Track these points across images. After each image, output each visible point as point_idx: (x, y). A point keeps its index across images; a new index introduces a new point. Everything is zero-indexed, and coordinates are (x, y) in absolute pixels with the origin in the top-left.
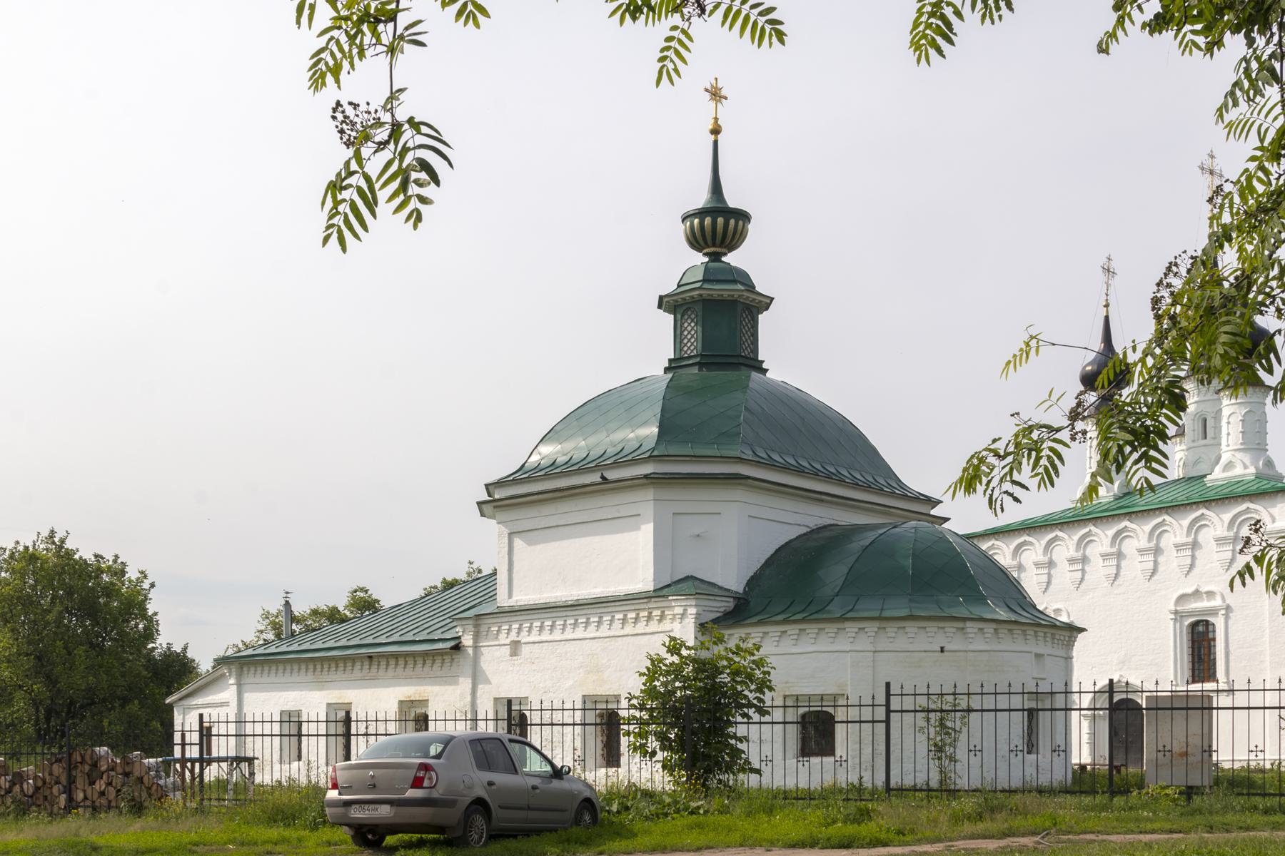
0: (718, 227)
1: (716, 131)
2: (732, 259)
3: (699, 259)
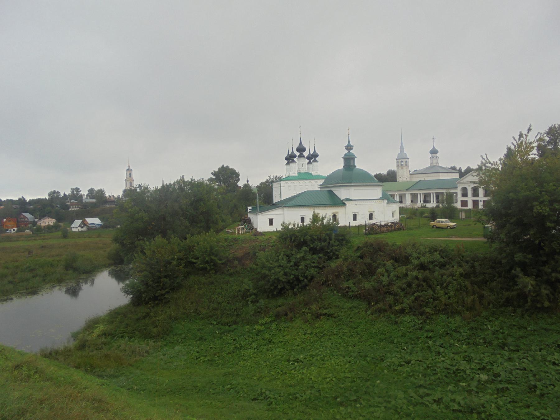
0: (349, 147)
2: (351, 151)
3: (347, 151)
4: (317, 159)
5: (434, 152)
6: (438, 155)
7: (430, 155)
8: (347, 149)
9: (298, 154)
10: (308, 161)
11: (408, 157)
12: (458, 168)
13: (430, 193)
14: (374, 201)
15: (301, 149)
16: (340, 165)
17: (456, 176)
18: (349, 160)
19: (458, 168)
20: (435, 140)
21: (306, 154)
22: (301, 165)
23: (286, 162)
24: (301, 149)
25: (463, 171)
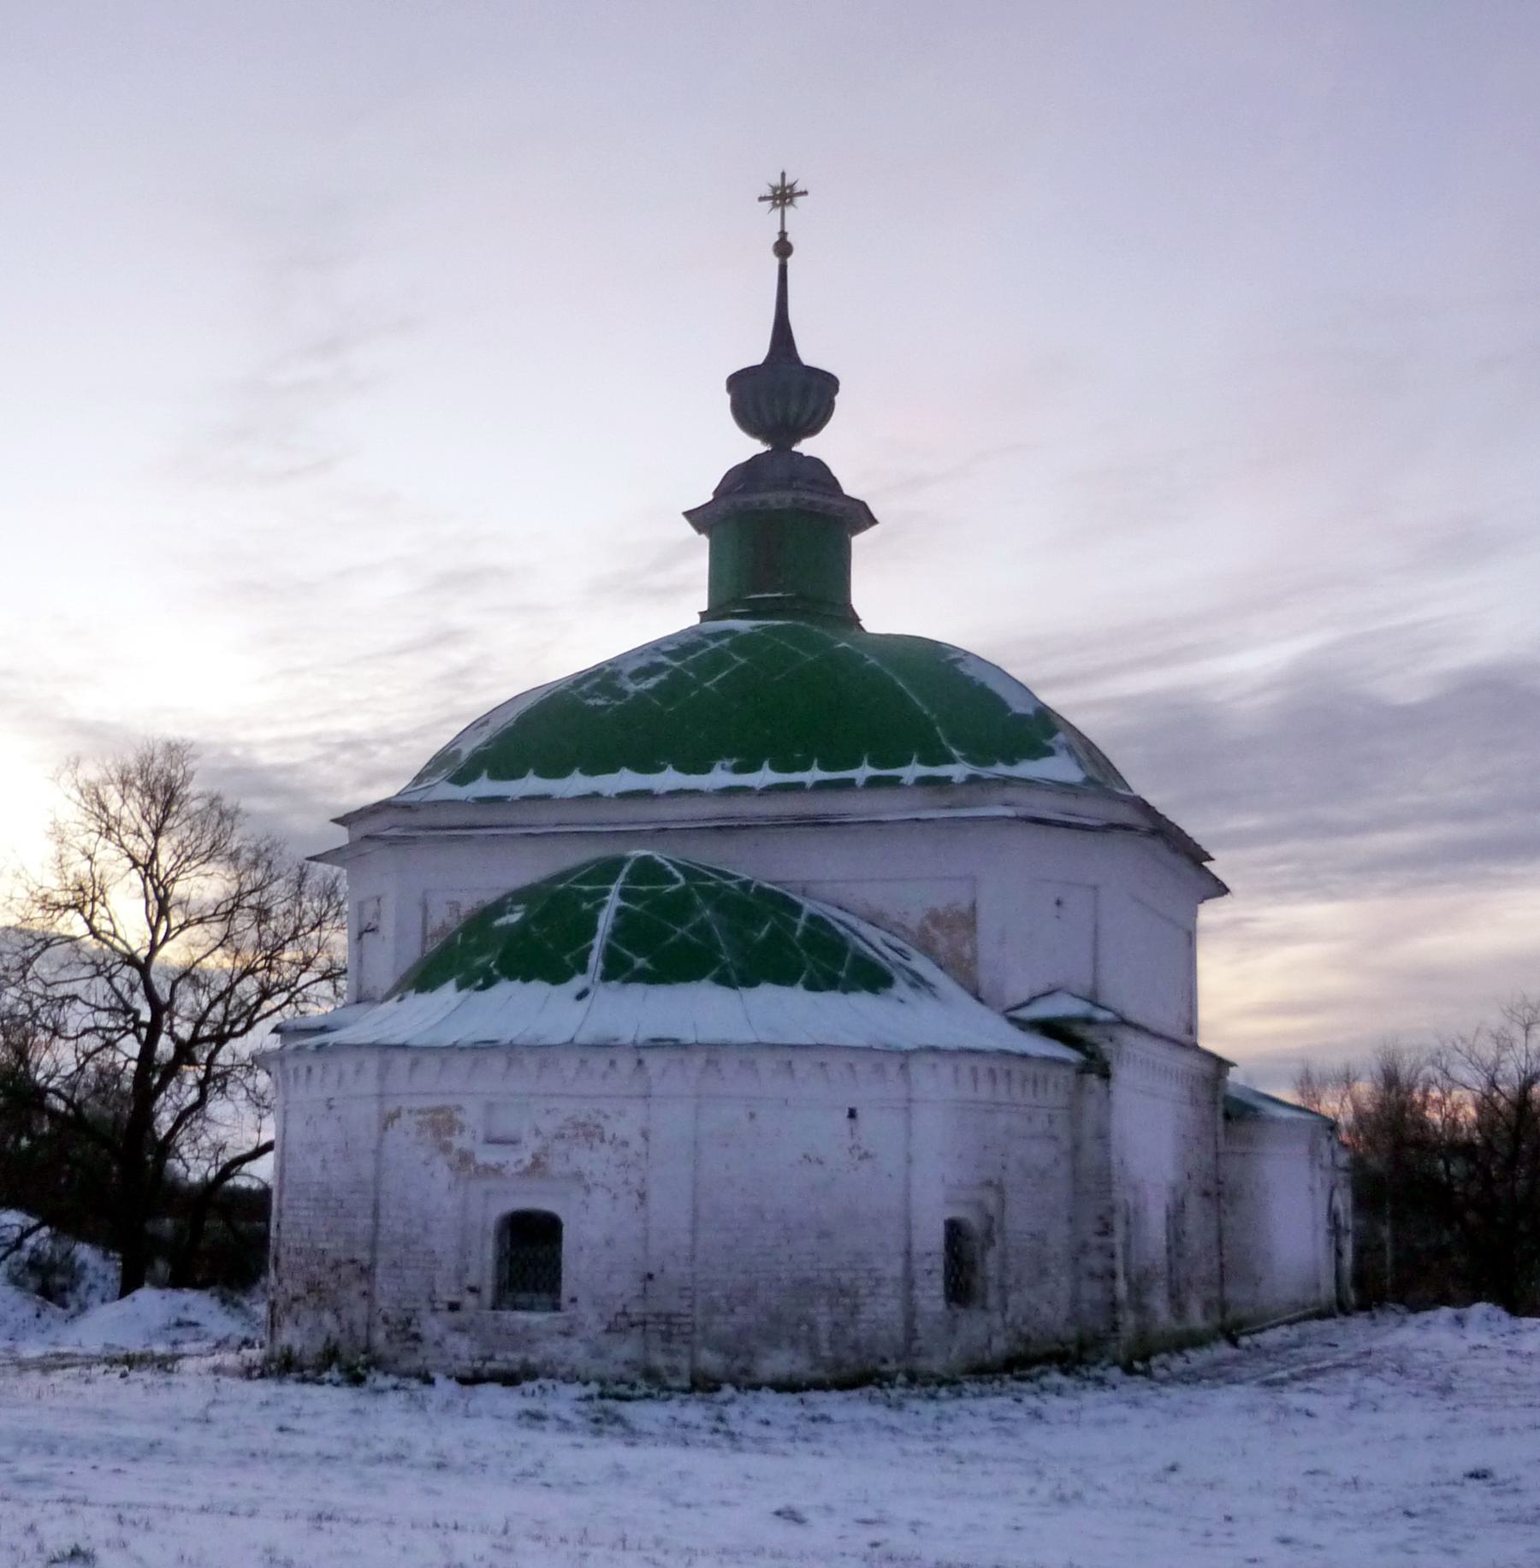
0: (782, 394)
1: (783, 249)
2: (806, 447)
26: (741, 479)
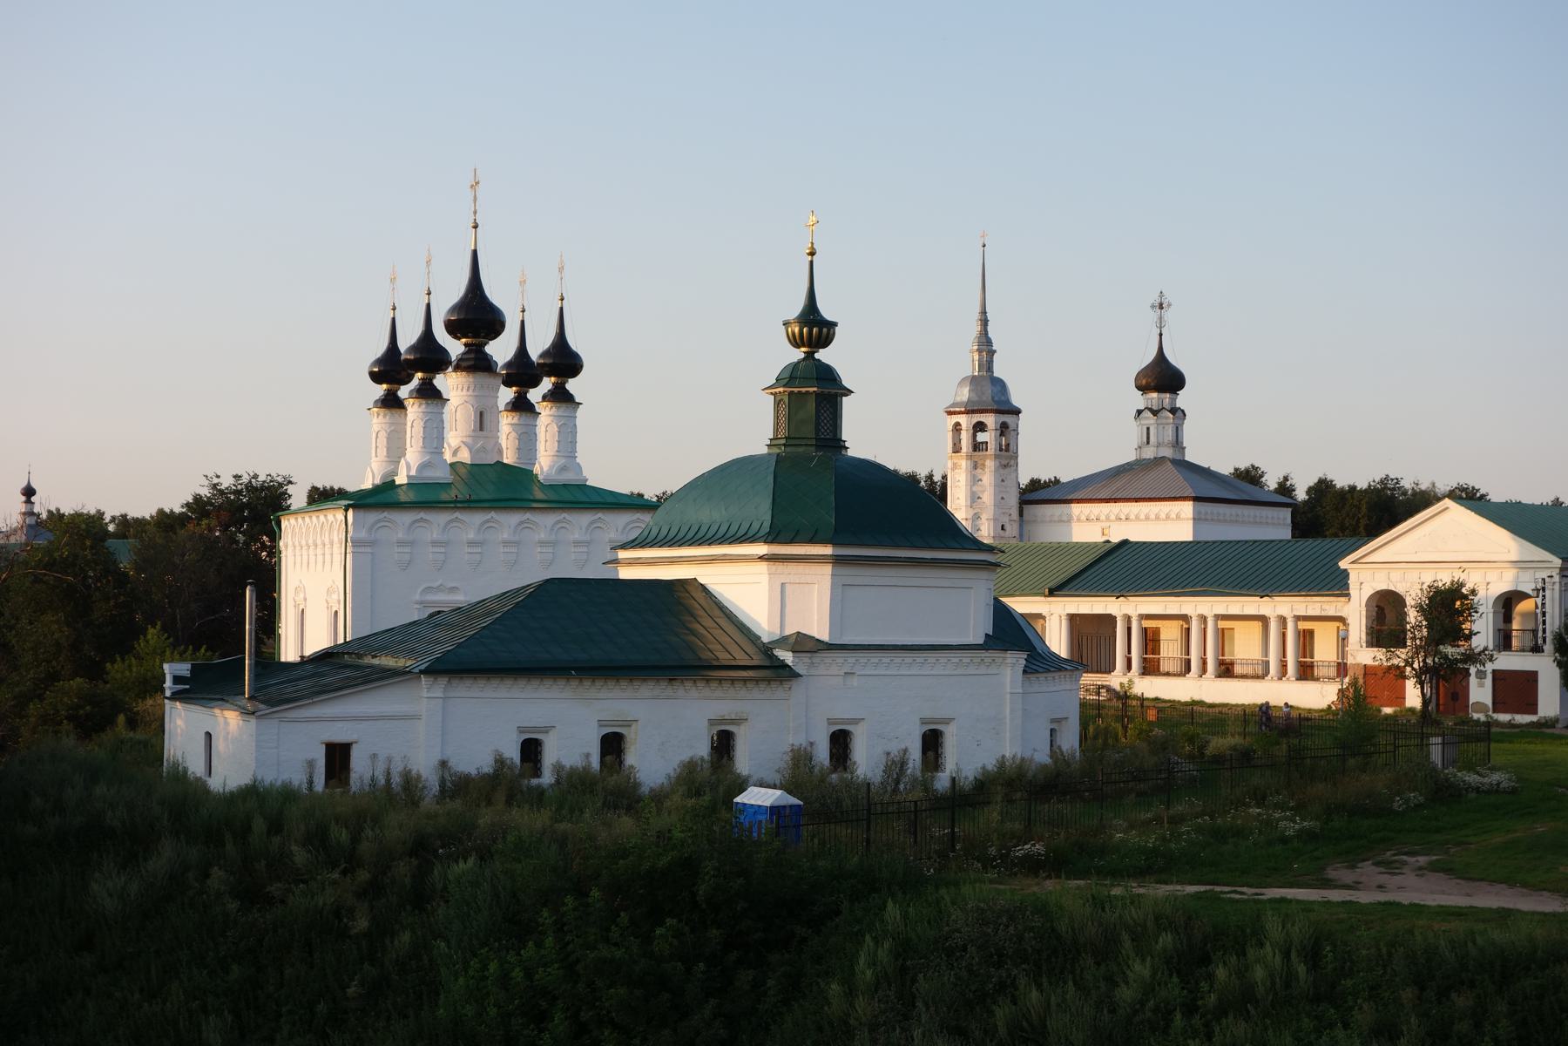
0: (814, 329)
2: (822, 355)
3: (798, 354)
4: (572, 385)
5: (1163, 378)
6: (1183, 399)
7: (1139, 400)
8: (796, 342)
9: (456, 348)
10: (507, 394)
11: (1016, 401)
12: (1271, 482)
13: (1110, 620)
14: (955, 656)
15: (477, 316)
16: (752, 430)
17: (1276, 527)
18: (812, 396)
19: (1271, 482)
20: (1168, 315)
21: (501, 350)
22: (461, 420)
23: (381, 390)
24: (477, 316)
25: (1301, 495)
26: (791, 376)
